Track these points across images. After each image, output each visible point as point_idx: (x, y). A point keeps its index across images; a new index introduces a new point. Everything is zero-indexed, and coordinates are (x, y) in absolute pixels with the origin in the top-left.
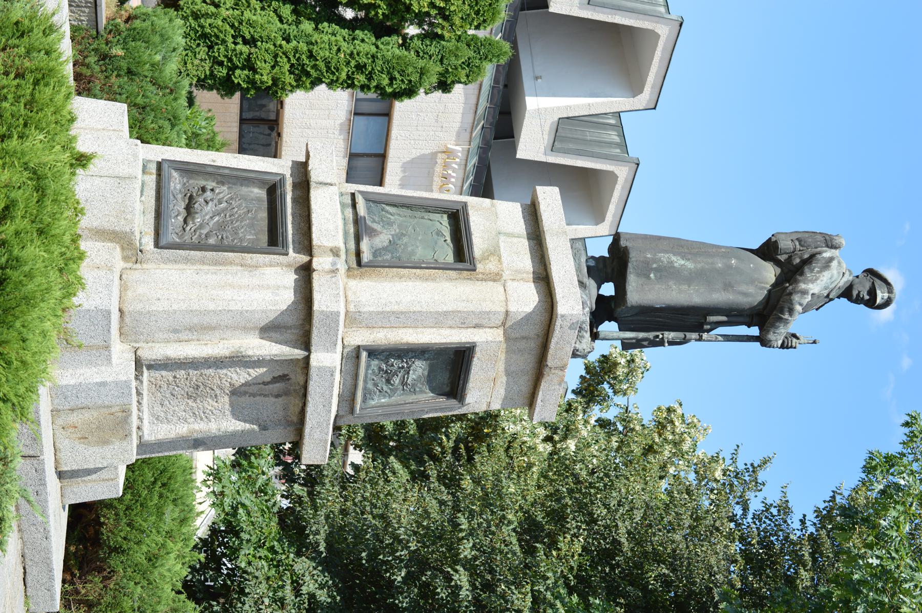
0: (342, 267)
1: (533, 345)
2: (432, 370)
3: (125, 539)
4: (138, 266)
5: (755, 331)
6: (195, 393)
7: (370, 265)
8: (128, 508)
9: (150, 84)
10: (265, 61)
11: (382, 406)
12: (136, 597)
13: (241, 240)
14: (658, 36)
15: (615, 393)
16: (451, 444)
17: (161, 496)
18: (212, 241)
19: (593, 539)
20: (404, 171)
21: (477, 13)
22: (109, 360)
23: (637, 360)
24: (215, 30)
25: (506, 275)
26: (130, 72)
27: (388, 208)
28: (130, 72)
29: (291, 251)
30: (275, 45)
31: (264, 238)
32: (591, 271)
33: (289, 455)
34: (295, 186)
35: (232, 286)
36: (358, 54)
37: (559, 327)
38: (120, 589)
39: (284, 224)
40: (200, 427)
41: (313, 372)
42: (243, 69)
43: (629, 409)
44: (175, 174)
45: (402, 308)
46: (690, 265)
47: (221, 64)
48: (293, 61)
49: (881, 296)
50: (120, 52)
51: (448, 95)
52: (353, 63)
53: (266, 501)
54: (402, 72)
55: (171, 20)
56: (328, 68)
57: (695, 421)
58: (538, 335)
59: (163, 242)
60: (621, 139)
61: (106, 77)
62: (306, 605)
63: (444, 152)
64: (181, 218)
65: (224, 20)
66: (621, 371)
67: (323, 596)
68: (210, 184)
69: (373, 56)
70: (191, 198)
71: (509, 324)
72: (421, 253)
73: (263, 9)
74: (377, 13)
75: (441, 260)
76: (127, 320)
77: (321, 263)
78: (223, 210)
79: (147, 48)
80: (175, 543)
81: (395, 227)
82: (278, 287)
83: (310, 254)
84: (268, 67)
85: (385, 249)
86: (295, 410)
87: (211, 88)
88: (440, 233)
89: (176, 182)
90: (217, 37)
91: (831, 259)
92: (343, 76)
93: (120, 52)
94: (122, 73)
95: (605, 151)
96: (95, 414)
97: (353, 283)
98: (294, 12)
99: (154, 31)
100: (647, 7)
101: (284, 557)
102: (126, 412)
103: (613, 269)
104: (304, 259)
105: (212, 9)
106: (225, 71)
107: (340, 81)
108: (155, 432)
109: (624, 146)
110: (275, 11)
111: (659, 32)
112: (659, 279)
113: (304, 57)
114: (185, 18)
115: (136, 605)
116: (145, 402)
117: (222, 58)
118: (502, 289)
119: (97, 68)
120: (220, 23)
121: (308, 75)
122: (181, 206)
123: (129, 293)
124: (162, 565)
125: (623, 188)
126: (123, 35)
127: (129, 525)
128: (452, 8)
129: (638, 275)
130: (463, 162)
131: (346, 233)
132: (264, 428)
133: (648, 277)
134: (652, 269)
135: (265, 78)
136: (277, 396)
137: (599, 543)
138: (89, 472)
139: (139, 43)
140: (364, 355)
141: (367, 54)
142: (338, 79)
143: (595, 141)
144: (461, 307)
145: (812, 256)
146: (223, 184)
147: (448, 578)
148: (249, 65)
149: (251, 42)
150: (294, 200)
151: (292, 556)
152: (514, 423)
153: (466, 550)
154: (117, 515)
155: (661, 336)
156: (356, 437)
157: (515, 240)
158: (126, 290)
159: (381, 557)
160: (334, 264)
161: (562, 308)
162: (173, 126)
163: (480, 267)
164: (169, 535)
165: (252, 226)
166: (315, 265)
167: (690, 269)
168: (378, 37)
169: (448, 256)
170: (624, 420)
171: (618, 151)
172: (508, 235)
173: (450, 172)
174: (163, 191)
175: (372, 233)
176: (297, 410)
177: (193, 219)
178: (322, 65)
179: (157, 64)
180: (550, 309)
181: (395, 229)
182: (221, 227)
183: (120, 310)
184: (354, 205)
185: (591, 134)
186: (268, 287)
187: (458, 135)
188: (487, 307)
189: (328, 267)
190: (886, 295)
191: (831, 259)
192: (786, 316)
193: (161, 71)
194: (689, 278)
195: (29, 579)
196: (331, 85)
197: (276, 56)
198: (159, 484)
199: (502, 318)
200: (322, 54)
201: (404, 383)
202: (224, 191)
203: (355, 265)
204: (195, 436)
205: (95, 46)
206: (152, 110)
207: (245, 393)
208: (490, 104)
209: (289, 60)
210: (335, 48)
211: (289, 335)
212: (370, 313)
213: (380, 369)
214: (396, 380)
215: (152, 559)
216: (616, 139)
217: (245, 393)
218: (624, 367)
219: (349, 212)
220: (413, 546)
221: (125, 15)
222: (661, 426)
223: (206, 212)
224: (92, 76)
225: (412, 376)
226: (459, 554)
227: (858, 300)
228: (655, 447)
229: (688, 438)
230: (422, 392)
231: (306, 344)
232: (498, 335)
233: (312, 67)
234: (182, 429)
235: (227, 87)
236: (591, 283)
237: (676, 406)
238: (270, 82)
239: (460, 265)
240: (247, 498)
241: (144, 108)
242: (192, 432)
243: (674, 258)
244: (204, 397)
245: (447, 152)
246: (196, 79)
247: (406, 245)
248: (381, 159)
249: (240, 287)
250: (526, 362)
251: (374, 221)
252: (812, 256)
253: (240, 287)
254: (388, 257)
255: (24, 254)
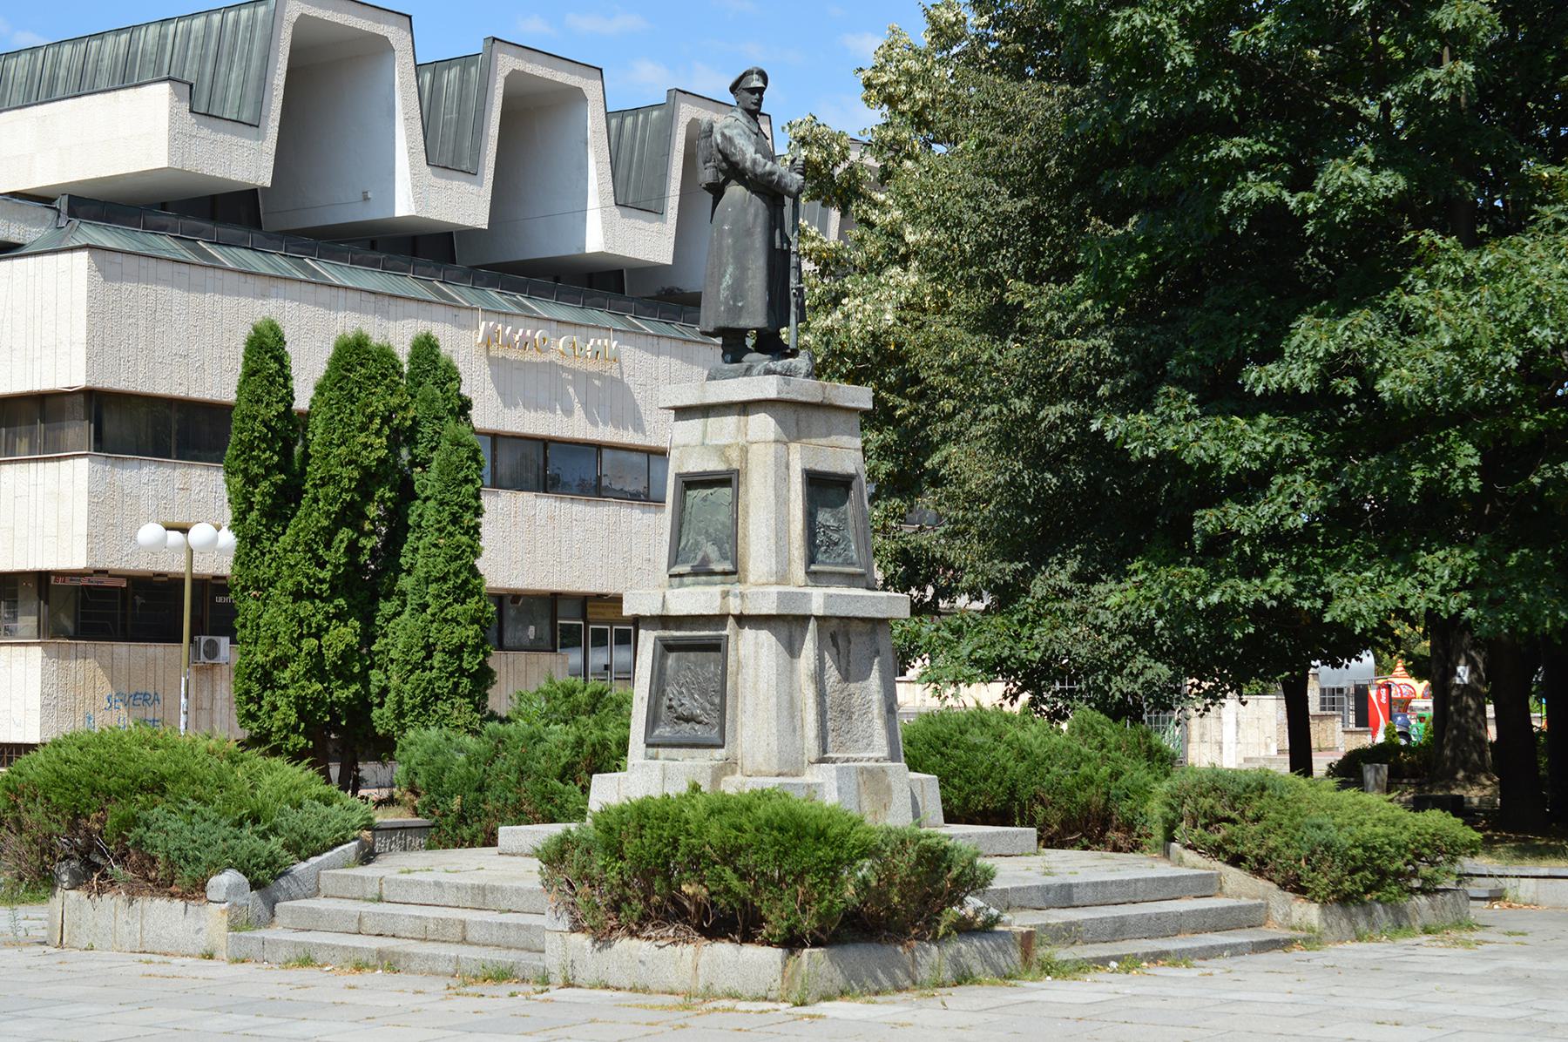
0: (738, 588)
1: (803, 414)
2: (825, 505)
3: (1000, 784)
4: (739, 762)
5: (788, 201)
6: (846, 713)
7: (735, 562)
8: (968, 781)
9: (494, 766)
10: (452, 633)
11: (858, 548)
12: (1062, 772)
13: (716, 675)
14: (303, 17)
15: (844, 158)
16: (906, 403)
17: (956, 747)
18: (717, 700)
19: (1018, 240)
20: (516, 406)
21: (384, 376)
22: (819, 785)
23: (802, 133)
24: (417, 692)
25: (742, 441)
26: (480, 789)
27: (682, 544)
28: (480, 789)
29: (724, 633)
30: (432, 622)
31: (713, 655)
32: (737, 359)
33: (925, 591)
34: (665, 628)
35: (755, 683)
36: (439, 522)
38: (1054, 789)
39: (701, 638)
40: (877, 708)
41: (828, 613)
42: (461, 660)
43: (866, 141)
44: (657, 732)
45: (773, 536)
46: (730, 270)
47: (456, 685)
48: (450, 599)
49: (756, 83)
50: (457, 800)
51: (474, 403)
52: (450, 528)
53: (969, 626)
54: (459, 469)
55: (411, 744)
56: (458, 558)
57: (881, 52)
59: (719, 742)
60: (456, 65)
61: (487, 815)
62: (1083, 585)
63: (488, 347)
64: (697, 727)
65: (405, 681)
66: (816, 156)
67: (1073, 565)
68: (665, 702)
69: (441, 504)
70: (677, 718)
72: (723, 517)
73: (385, 636)
74: (389, 499)
75: (730, 499)
76: (786, 770)
77: (734, 607)
78: (689, 690)
79: (450, 770)
80: (1007, 732)
81: (699, 539)
82: (757, 644)
83: (728, 615)
84: (458, 630)
85: (720, 549)
86: (861, 627)
87: (485, 696)
88: (705, 499)
89: (664, 731)
90: (425, 689)
91: (723, 135)
92: (465, 539)
93: (457, 800)
94: (481, 798)
95: (473, 89)
96: (864, 796)
97: (751, 578)
98: (387, 598)
99: (431, 762)
100: (258, 33)
101: (1031, 609)
102: (863, 771)
104: (731, 621)
105: (392, 695)
106: (465, 680)
107: (471, 542)
108: (880, 747)
109: (466, 61)
110: (388, 621)
111: (297, 15)
112: (743, 298)
113: (445, 587)
114: (403, 728)
115: (1071, 771)
116: (854, 756)
117: (450, 684)
118: (755, 446)
119: (476, 826)
120: (408, 687)
121: (466, 582)
122: (686, 727)
123: (763, 769)
124: (1030, 745)
125: (530, 61)
126: (436, 797)
127: (986, 780)
128: (382, 408)
129: (740, 317)
130: (502, 318)
131: (707, 584)
132: (877, 653)
135: (471, 633)
136: (850, 642)
137: (1023, 233)
138: (915, 804)
139: (445, 780)
140: (813, 568)
141: (439, 512)
142: (469, 546)
143: (459, 105)
144: (771, 482)
145: (720, 151)
146: (664, 690)
147: (1053, 427)
148: (457, 651)
149: (429, 650)
150: (678, 629)
151: (1028, 600)
152: (884, 311)
153: (1023, 405)
154: (975, 793)
156: (901, 508)
157: (709, 429)
158: (760, 772)
159: (1030, 501)
160: (735, 596)
161: (772, 394)
162: (541, 740)
163: (735, 466)
164: (998, 737)
165: (702, 666)
166: (737, 612)
168: (416, 497)
169: (727, 491)
170: (881, 148)
171: (473, 69)
172: (704, 438)
173: (517, 338)
174: (673, 742)
175: (706, 560)
176: (861, 624)
177: (698, 716)
178: (454, 566)
179: (468, 757)
181: (702, 539)
182: (704, 693)
183: (778, 775)
184: (681, 575)
185: (448, 111)
186: (756, 652)
187: (464, 327)
188: (771, 460)
189: (738, 601)
190: (755, 76)
191: (723, 135)
192: (776, 177)
193: (478, 753)
194: (742, 269)
195: (1005, 852)
196: (476, 554)
197: (445, 620)
198: (943, 749)
199: (780, 446)
200: (441, 566)
201: (837, 530)
202: (671, 690)
203: (735, 577)
204: (884, 712)
205: (449, 829)
206: (525, 763)
207: (847, 670)
208: (409, 272)
209: (449, 604)
210: (433, 549)
211: (797, 633)
212: (777, 562)
213: (826, 552)
214: (835, 537)
215: (1022, 755)
216: (455, 72)
217: (847, 670)
218: (811, 152)
219: (687, 580)
220: (1019, 465)
221: (409, 796)
222: (891, 100)
223: (689, 705)
224: (486, 832)
225: (831, 523)
226: (1026, 414)
227: (759, 103)
228: (916, 109)
229: (905, 63)
230: (845, 513)
231: (805, 619)
232: (795, 447)
233: (457, 577)
234: (878, 726)
235: (483, 678)
236: (748, 358)
237: (862, 76)
238: (476, 626)
239: (734, 483)
240: (964, 649)
241: (522, 772)
242: (880, 715)
243: (724, 285)
244: (850, 706)
245: (489, 341)
246: (475, 714)
247: (716, 530)
248: (499, 440)
249: (757, 676)
250: (818, 418)
251: (695, 558)
252: (720, 151)
253: (757, 676)
254: (727, 546)
255: (763, 817)
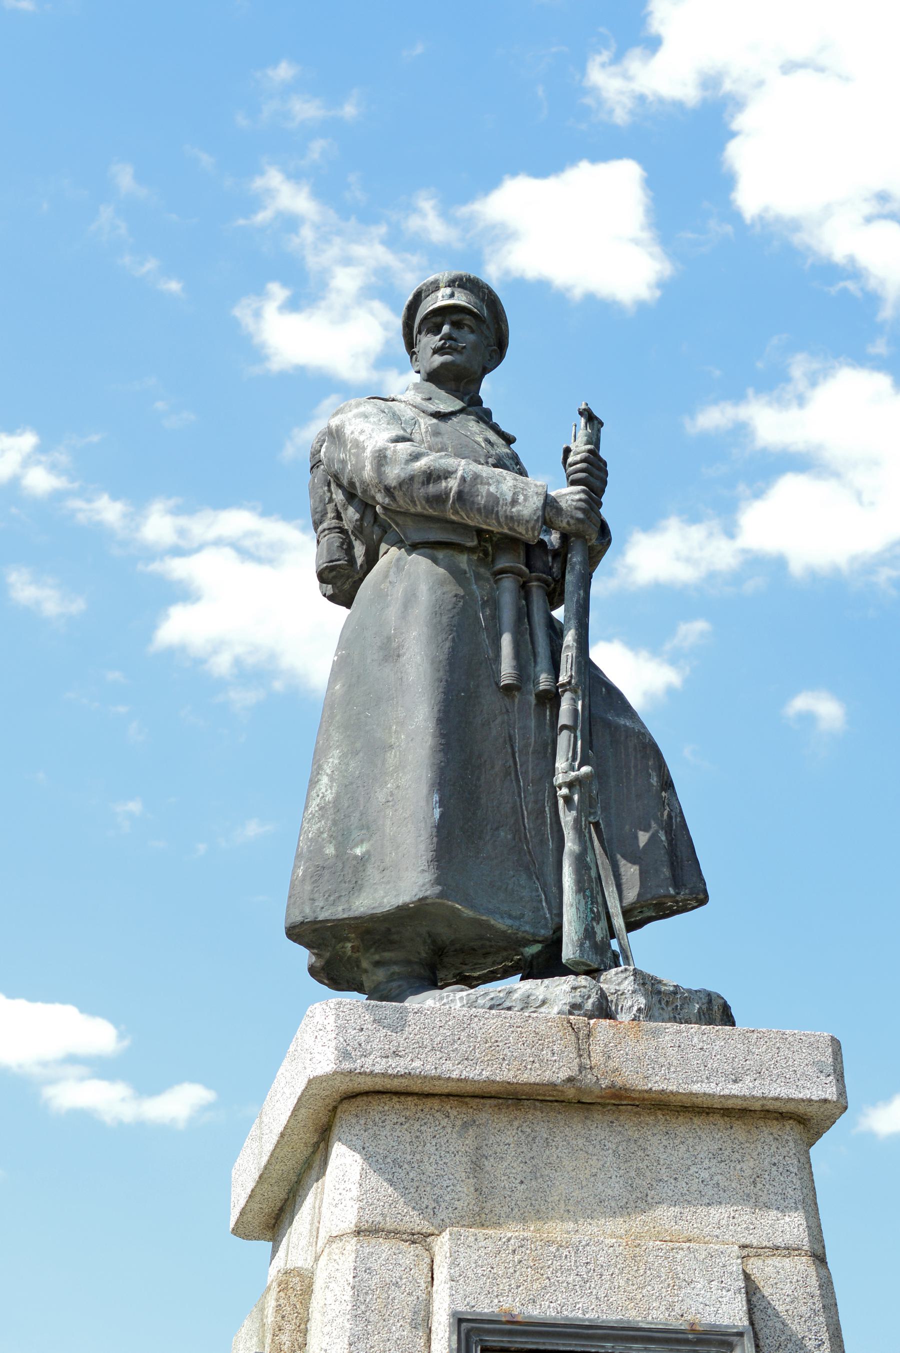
37: (392, 1062)
58: (465, 1126)
71: (416, 1222)
103: (377, 964)
112: (368, 828)
129: (357, 887)
133: (363, 860)
134: (341, 854)
155: (564, 791)
167: (344, 756)
180: (359, 1101)
